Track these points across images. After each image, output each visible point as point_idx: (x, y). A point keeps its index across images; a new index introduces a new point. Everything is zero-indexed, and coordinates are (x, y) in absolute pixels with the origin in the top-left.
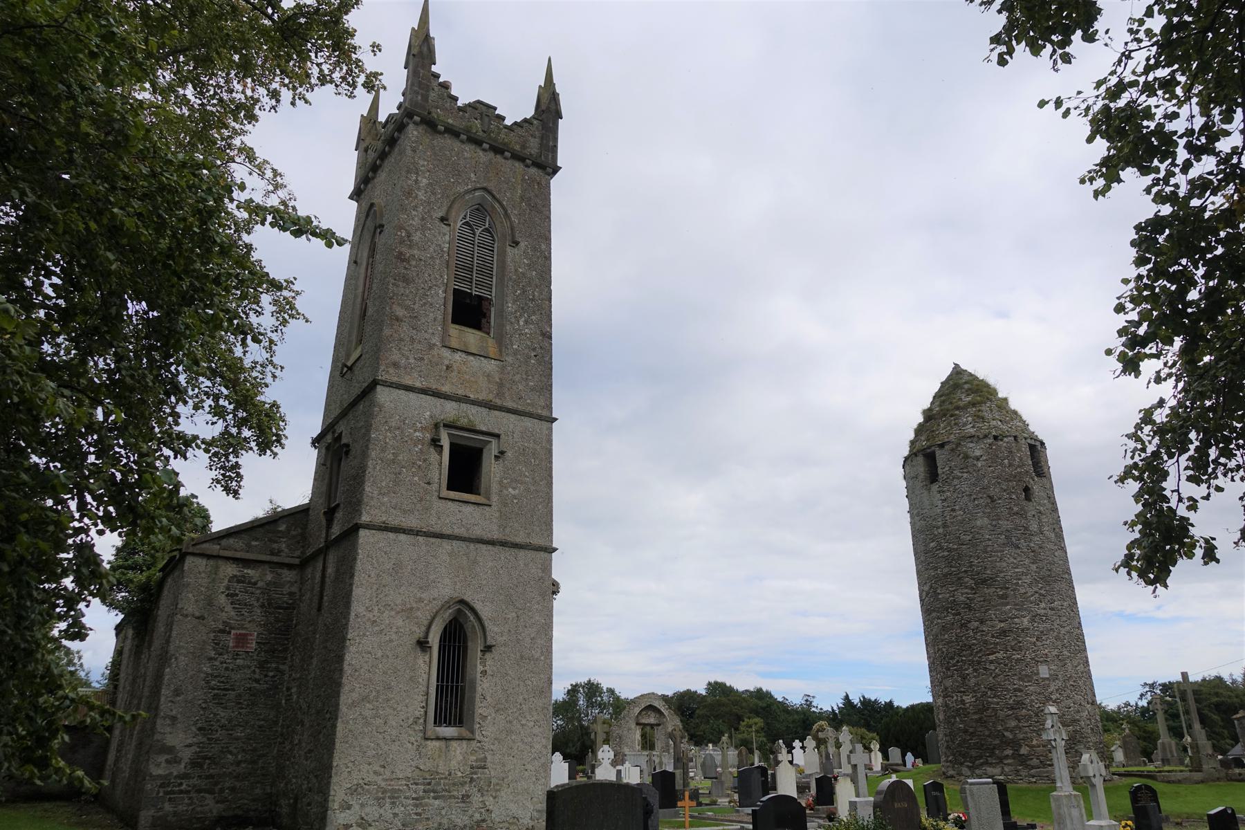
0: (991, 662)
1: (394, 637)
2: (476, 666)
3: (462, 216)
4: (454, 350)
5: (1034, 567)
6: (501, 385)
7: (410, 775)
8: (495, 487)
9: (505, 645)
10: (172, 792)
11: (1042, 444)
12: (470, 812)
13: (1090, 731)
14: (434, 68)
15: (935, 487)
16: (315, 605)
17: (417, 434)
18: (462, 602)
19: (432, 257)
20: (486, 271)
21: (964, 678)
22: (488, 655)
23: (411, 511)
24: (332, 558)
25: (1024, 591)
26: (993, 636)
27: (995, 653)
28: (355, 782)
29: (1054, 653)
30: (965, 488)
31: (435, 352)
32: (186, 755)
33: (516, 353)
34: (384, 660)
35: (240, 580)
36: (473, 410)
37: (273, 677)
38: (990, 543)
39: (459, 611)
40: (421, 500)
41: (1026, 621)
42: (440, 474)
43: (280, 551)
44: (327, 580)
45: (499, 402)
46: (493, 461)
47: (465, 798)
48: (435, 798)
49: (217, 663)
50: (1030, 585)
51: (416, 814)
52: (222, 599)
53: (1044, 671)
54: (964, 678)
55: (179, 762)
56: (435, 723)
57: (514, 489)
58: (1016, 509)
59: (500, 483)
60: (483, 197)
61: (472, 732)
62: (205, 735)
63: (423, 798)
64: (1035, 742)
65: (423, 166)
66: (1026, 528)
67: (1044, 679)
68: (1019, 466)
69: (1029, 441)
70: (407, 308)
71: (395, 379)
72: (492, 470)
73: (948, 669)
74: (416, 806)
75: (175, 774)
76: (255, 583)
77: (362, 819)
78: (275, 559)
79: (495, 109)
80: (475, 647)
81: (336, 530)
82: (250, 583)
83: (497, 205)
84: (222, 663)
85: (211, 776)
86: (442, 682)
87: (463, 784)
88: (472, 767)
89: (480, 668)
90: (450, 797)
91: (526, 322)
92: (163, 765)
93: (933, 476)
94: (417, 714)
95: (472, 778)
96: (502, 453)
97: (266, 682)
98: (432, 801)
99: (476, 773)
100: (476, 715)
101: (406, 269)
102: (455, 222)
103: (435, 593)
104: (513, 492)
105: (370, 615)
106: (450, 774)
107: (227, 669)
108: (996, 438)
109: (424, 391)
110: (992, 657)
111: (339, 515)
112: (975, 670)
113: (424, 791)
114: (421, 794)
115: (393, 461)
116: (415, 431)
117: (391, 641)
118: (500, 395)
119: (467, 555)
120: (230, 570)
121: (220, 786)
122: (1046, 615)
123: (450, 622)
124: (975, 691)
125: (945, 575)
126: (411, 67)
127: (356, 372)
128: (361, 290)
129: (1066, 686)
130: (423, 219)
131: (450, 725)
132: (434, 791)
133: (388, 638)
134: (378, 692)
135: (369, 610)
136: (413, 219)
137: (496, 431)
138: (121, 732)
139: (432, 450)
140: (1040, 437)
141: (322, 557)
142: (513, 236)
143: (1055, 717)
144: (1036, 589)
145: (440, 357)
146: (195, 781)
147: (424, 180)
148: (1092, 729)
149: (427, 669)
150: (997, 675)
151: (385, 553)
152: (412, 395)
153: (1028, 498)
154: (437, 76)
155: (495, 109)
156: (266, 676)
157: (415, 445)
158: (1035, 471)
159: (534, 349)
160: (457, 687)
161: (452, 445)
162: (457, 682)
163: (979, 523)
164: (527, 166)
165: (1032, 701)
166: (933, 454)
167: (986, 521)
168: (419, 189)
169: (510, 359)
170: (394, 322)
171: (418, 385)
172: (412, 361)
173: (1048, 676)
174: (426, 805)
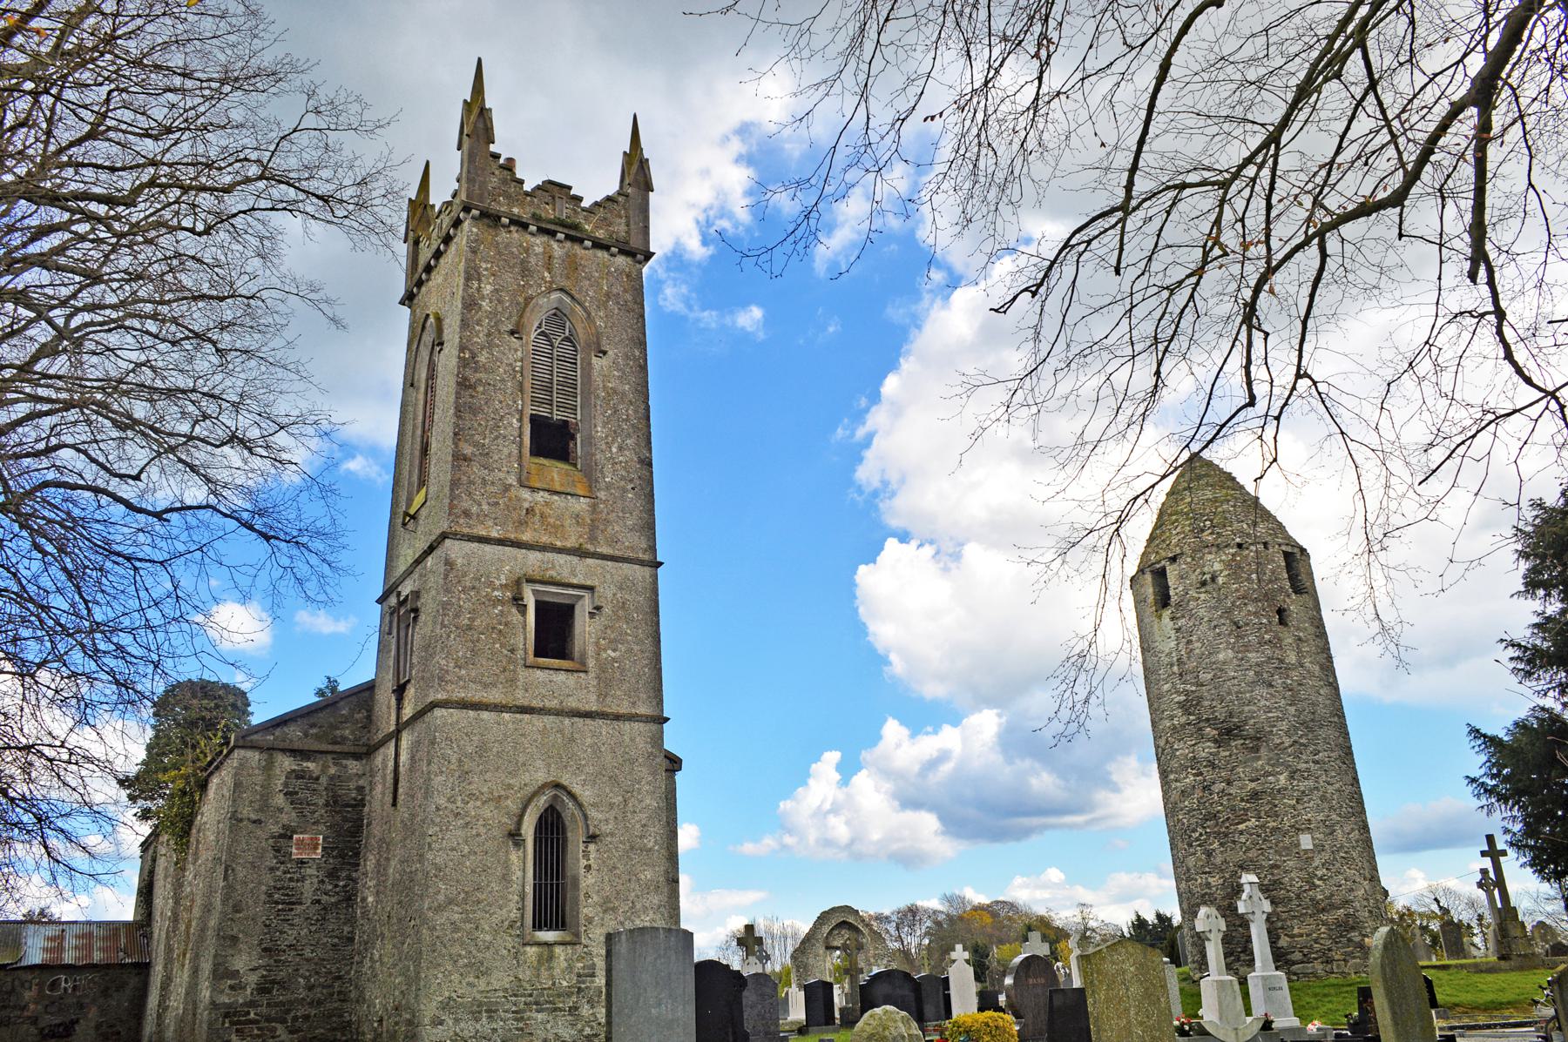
0: (1241, 833)
1: (482, 830)
2: (578, 860)
3: (536, 324)
4: (534, 490)
5: (1292, 710)
6: (593, 527)
7: (507, 986)
8: (591, 650)
9: (612, 834)
10: (239, 1022)
11: (1303, 551)
12: (579, 1026)
13: (1367, 914)
14: (493, 148)
15: (1167, 613)
16: (389, 799)
17: (496, 593)
18: (558, 786)
19: (503, 380)
20: (569, 386)
21: (1209, 854)
22: (592, 847)
23: (494, 685)
24: (406, 739)
25: (1278, 741)
26: (1242, 800)
27: (1245, 821)
28: (447, 994)
29: (1319, 818)
30: (1202, 612)
31: (513, 492)
32: (253, 979)
33: (608, 487)
34: (472, 858)
35: (299, 775)
36: (561, 559)
37: (345, 886)
38: (1236, 681)
39: (555, 797)
40: (504, 670)
41: (1283, 779)
42: (525, 639)
43: (344, 739)
44: (401, 769)
45: (591, 548)
46: (587, 619)
47: (574, 1009)
48: (538, 1011)
49: (278, 873)
50: (1287, 733)
51: (517, 1029)
52: (280, 800)
53: (1306, 842)
54: (1209, 854)
55: (244, 988)
56: (534, 926)
57: (614, 650)
58: (1267, 637)
59: (597, 643)
60: (560, 300)
61: (577, 935)
62: (271, 957)
63: (524, 1011)
64: (1296, 931)
65: (486, 269)
66: (1281, 661)
67: (1306, 851)
68: (1270, 581)
69: (1284, 548)
70: (476, 445)
71: (466, 530)
72: (585, 629)
73: (1190, 845)
74: (516, 1019)
75: (241, 1001)
76: (317, 778)
77: (456, 1034)
78: (337, 748)
79: (570, 188)
80: (576, 838)
81: (408, 712)
82: (311, 778)
83: (578, 308)
84: (285, 873)
85: (282, 1004)
86: (540, 879)
87: (569, 995)
88: (579, 975)
89: (583, 862)
90: (555, 1010)
91: (620, 448)
92: (227, 991)
93: (1164, 600)
94: (512, 915)
95: (579, 988)
96: (598, 608)
97: (337, 893)
98: (534, 1015)
99: (584, 982)
100: (581, 916)
101: (472, 397)
102: (528, 334)
103: (526, 778)
104: (613, 654)
105: (453, 807)
106: (554, 984)
107: (291, 880)
108: (1240, 546)
109: (501, 542)
110: (1242, 827)
111: (411, 692)
112: (1222, 845)
113: (525, 1004)
114: (522, 1006)
115: (470, 628)
116: (494, 589)
117: (478, 835)
118: (593, 539)
119: (561, 731)
120: (286, 763)
121: (292, 1014)
122: (1308, 770)
123: (546, 810)
124: (1222, 871)
125: (1183, 726)
126: (465, 146)
127: (421, 522)
128: (420, 418)
129: (1335, 859)
130: (489, 335)
131: (550, 929)
132: (537, 1003)
133: (474, 832)
134: (467, 893)
135: (451, 800)
136: (477, 336)
137: (589, 583)
138: (165, 967)
139: (514, 610)
140: (1301, 542)
141: (392, 743)
142: (599, 344)
143: (1256, 888)
144: (1295, 738)
145: (519, 499)
146: (264, 1010)
147: (488, 287)
148: (1370, 912)
149: (522, 865)
150: (1249, 849)
151: (467, 734)
152: (488, 548)
153: (1282, 622)
154: (496, 156)
155: (570, 188)
156: (336, 886)
157: (494, 607)
158: (1293, 586)
159: (631, 481)
160: (558, 885)
161: (537, 602)
162: (558, 879)
163: (1221, 656)
164: (613, 255)
165: (1292, 879)
166: (1163, 570)
167: (1230, 653)
168: (483, 298)
169: (602, 495)
170: (461, 462)
171: (494, 534)
172: (485, 507)
173: (1311, 847)
174: (529, 1019)
